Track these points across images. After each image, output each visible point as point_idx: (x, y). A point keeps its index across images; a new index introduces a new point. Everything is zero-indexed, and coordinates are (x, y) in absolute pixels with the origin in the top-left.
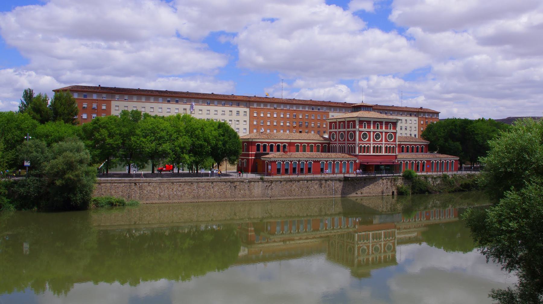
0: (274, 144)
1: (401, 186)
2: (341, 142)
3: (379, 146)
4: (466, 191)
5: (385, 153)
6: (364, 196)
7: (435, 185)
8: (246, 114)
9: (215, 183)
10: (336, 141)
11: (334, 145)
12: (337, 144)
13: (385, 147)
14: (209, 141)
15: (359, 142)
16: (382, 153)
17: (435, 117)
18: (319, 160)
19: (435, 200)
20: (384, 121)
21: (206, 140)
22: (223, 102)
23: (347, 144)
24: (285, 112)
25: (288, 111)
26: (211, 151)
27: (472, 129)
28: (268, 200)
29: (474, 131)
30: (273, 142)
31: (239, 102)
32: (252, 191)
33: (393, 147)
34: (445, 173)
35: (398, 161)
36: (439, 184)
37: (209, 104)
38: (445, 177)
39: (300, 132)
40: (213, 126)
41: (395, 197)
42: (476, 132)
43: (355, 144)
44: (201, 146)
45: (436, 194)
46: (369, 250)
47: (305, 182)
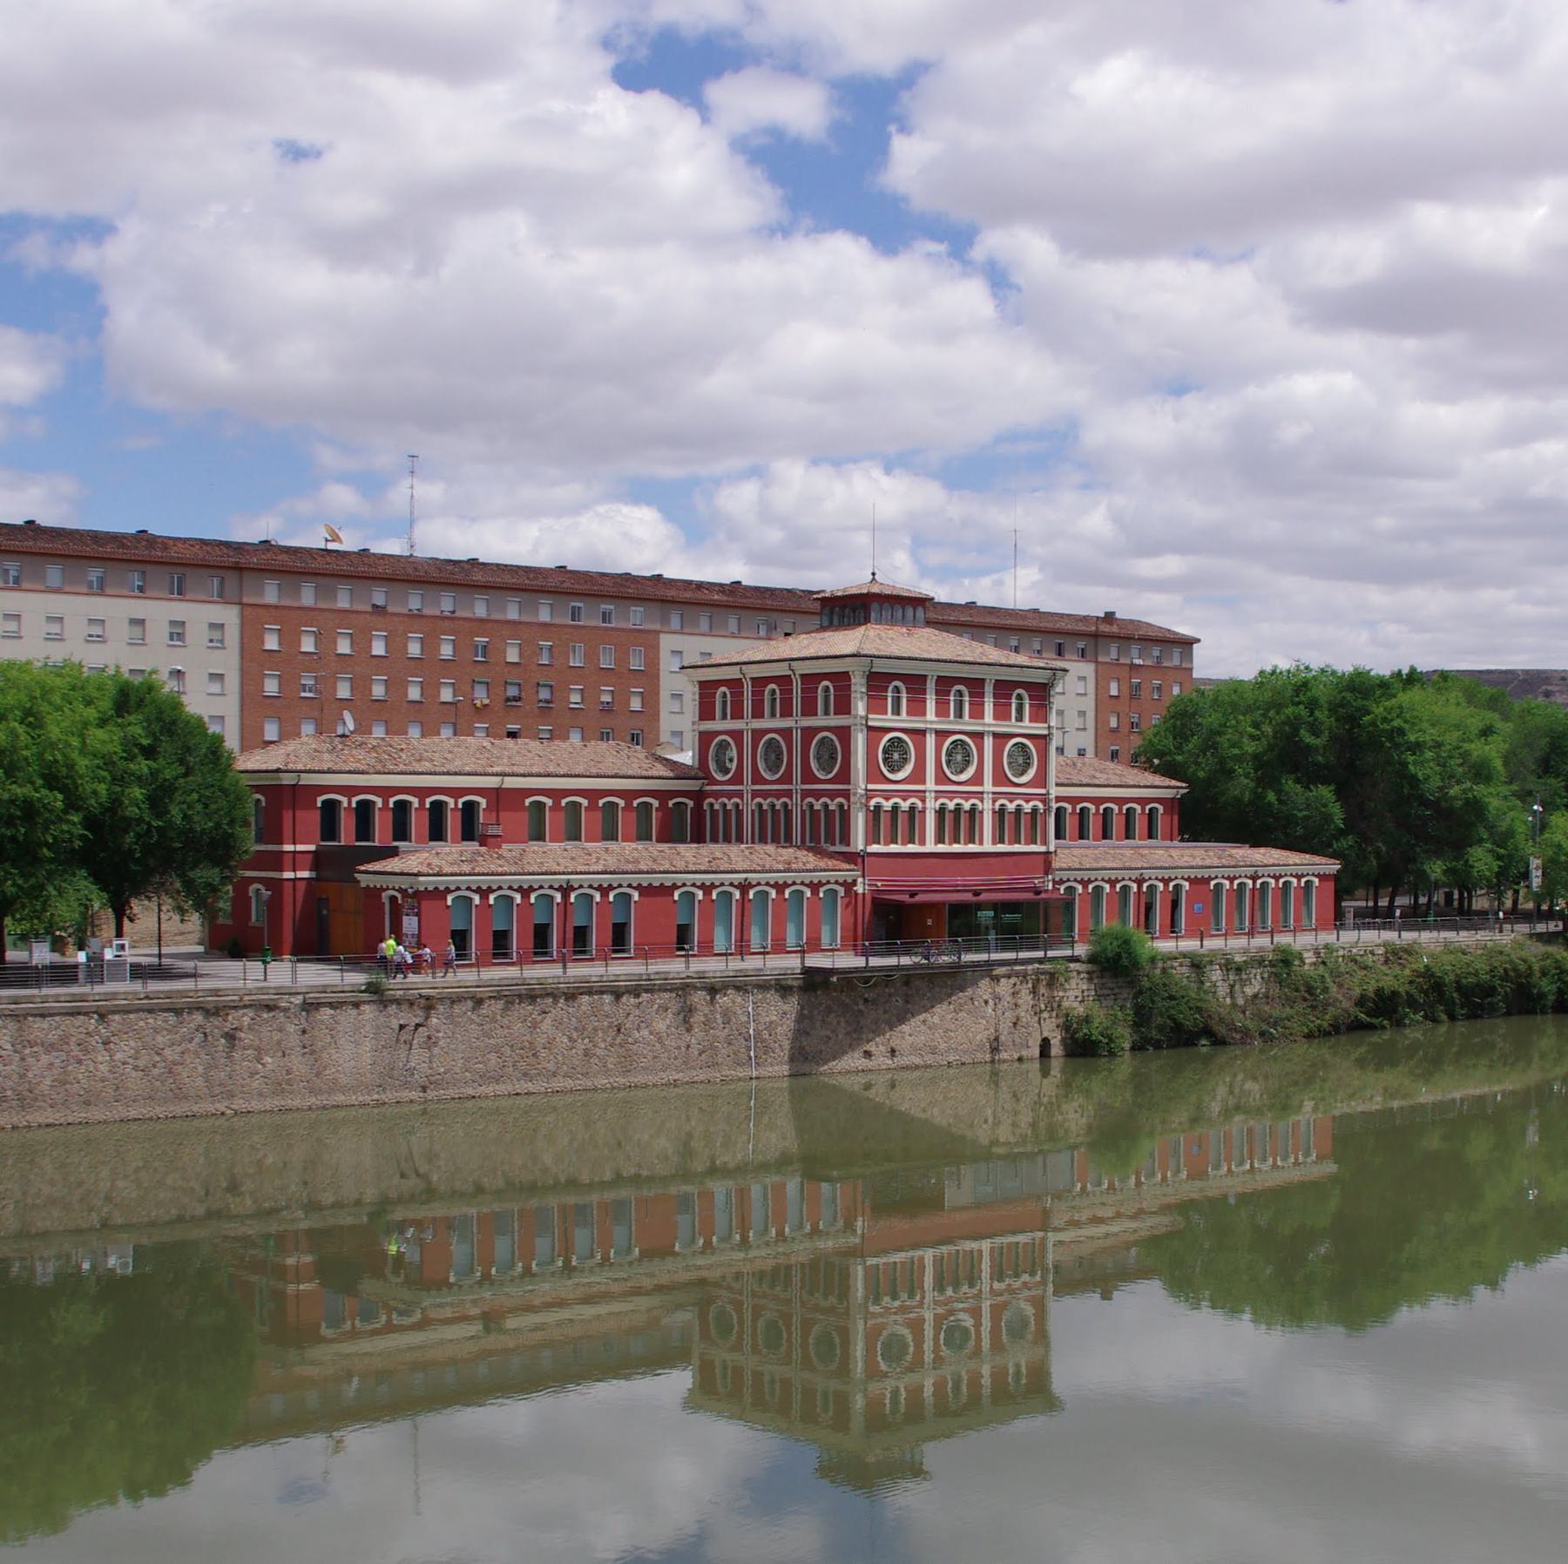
0: (415, 801)
1: (1081, 1010)
3: (967, 806)
4: (1383, 1028)
5: (994, 843)
6: (906, 1068)
7: (1240, 1001)
8: (222, 641)
9: (117, 1017)
10: (738, 779)
11: (726, 800)
12: (747, 796)
13: (994, 812)
14: (75, 783)
15: (870, 787)
16: (981, 843)
17: (1176, 661)
18: (668, 884)
19: (1240, 1077)
20: (991, 676)
21: (56, 778)
22: (94, 573)
23: (936, 799)
24: (432, 627)
25: (447, 624)
26: (82, 837)
27: (1395, 723)
28: (411, 1101)
29: (1401, 732)
31: (180, 569)
32: (325, 1055)
33: (1035, 810)
34: (1283, 939)
35: (1055, 882)
36: (1255, 996)
37: (17, 580)
38: (1286, 959)
39: (512, 735)
40: (89, 703)
41: (1056, 1065)
42: (1412, 738)
43: (846, 794)
44: (29, 811)
45: (1248, 1047)
46: (919, 1340)
47: (607, 998)
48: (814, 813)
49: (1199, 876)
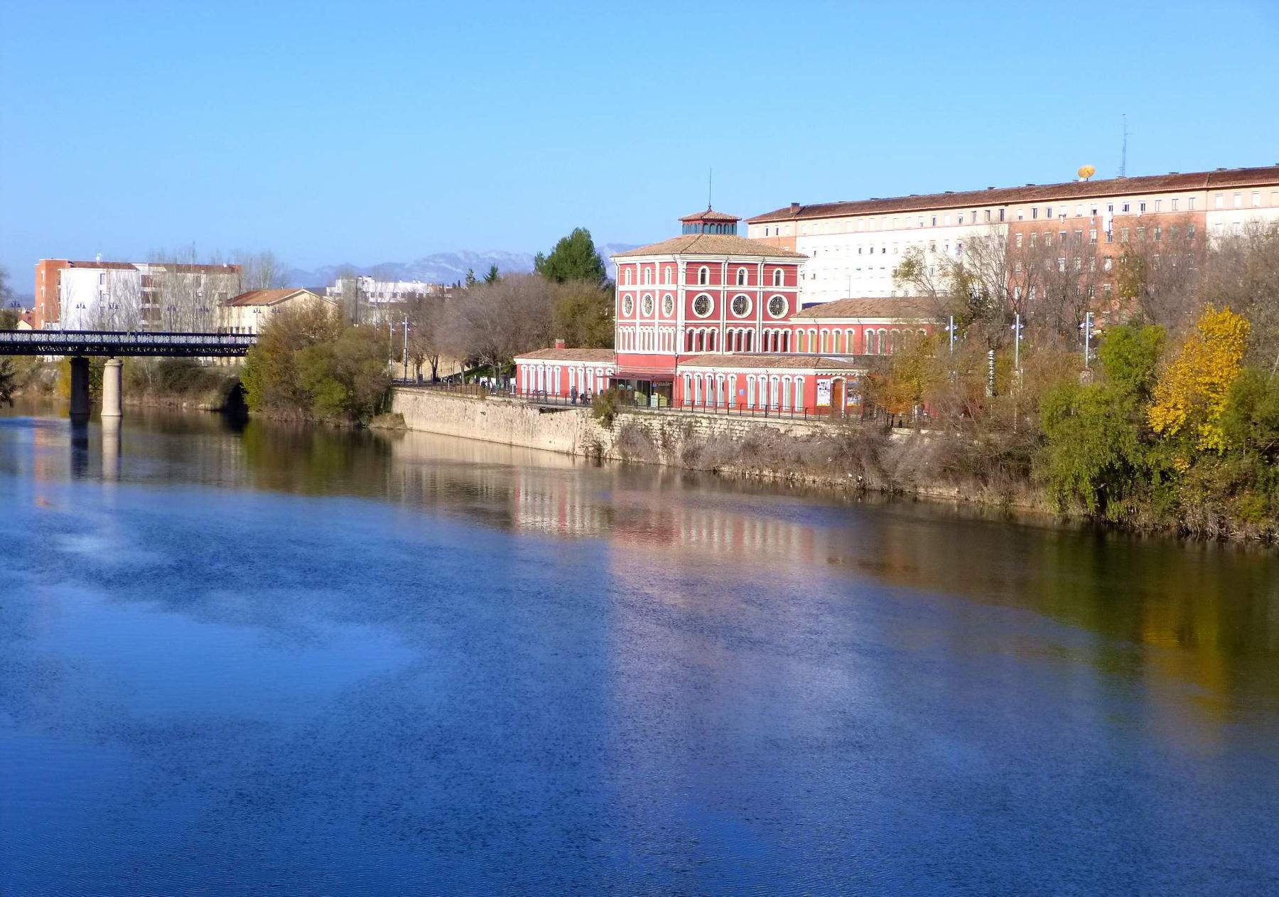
43: (676, 325)
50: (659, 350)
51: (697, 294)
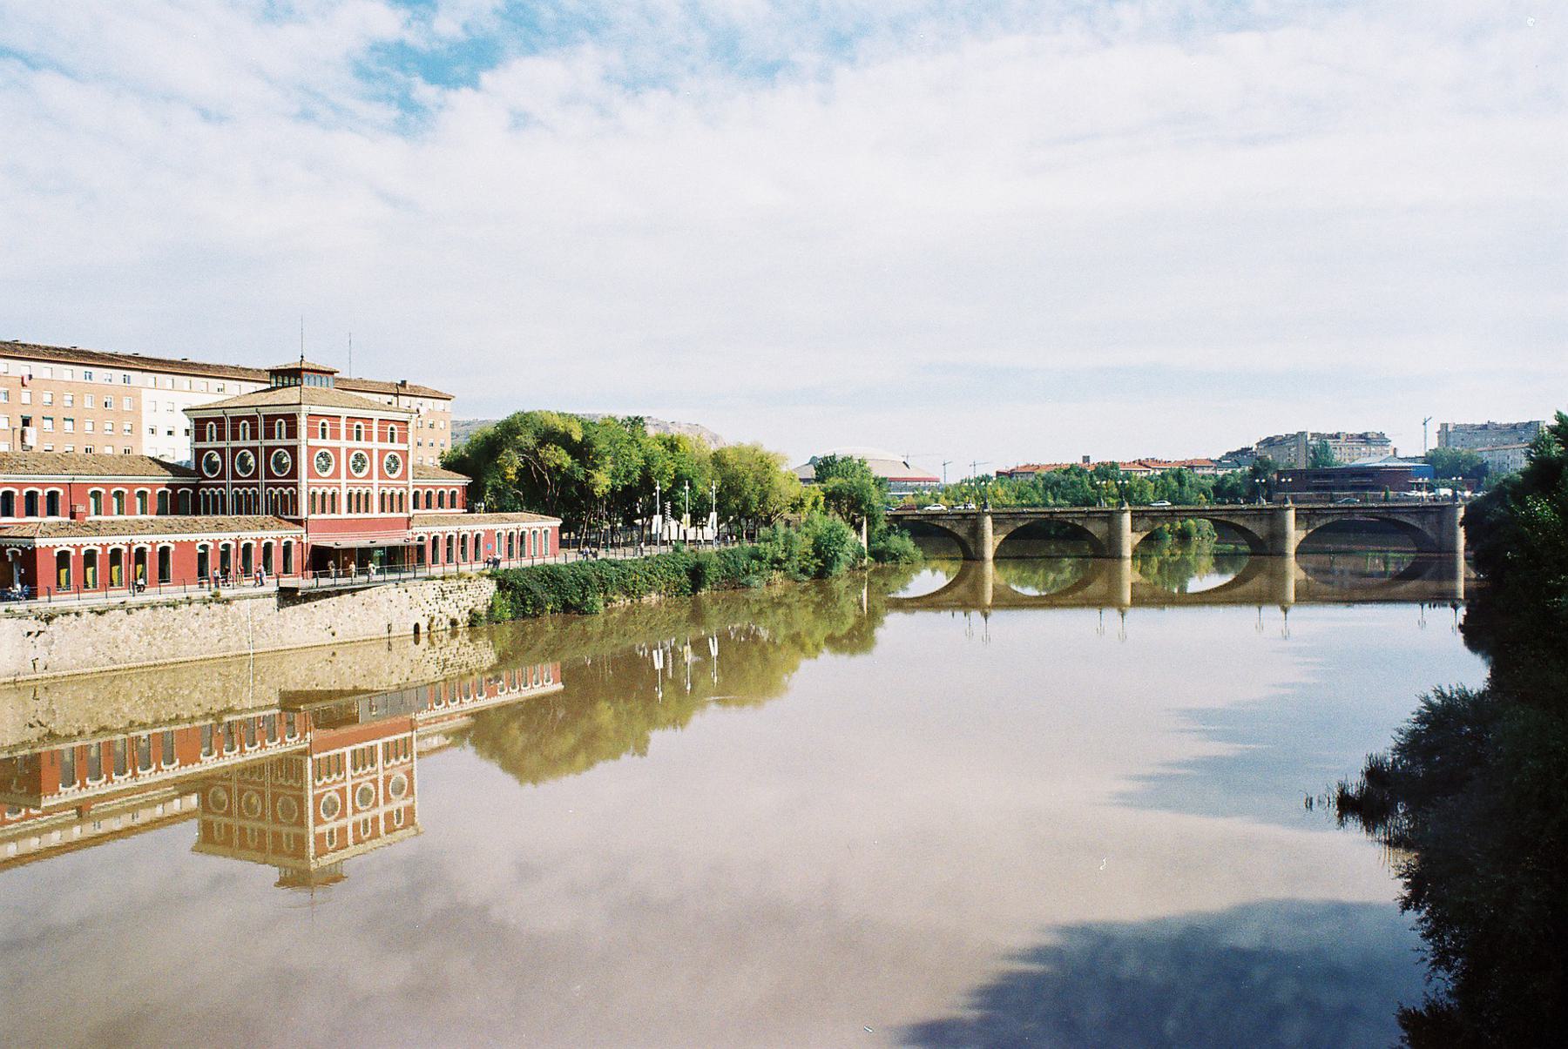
2: (209, 482)
10: (255, 476)
11: (214, 489)
15: (310, 481)
30: (432, 487)
43: (295, 485)
48: (239, 497)
49: (185, 540)
50: (350, 511)
51: (274, 450)
